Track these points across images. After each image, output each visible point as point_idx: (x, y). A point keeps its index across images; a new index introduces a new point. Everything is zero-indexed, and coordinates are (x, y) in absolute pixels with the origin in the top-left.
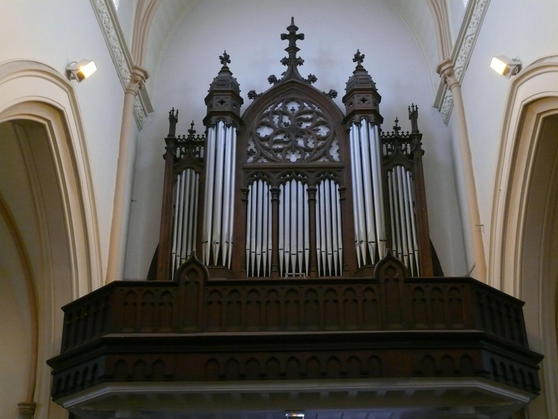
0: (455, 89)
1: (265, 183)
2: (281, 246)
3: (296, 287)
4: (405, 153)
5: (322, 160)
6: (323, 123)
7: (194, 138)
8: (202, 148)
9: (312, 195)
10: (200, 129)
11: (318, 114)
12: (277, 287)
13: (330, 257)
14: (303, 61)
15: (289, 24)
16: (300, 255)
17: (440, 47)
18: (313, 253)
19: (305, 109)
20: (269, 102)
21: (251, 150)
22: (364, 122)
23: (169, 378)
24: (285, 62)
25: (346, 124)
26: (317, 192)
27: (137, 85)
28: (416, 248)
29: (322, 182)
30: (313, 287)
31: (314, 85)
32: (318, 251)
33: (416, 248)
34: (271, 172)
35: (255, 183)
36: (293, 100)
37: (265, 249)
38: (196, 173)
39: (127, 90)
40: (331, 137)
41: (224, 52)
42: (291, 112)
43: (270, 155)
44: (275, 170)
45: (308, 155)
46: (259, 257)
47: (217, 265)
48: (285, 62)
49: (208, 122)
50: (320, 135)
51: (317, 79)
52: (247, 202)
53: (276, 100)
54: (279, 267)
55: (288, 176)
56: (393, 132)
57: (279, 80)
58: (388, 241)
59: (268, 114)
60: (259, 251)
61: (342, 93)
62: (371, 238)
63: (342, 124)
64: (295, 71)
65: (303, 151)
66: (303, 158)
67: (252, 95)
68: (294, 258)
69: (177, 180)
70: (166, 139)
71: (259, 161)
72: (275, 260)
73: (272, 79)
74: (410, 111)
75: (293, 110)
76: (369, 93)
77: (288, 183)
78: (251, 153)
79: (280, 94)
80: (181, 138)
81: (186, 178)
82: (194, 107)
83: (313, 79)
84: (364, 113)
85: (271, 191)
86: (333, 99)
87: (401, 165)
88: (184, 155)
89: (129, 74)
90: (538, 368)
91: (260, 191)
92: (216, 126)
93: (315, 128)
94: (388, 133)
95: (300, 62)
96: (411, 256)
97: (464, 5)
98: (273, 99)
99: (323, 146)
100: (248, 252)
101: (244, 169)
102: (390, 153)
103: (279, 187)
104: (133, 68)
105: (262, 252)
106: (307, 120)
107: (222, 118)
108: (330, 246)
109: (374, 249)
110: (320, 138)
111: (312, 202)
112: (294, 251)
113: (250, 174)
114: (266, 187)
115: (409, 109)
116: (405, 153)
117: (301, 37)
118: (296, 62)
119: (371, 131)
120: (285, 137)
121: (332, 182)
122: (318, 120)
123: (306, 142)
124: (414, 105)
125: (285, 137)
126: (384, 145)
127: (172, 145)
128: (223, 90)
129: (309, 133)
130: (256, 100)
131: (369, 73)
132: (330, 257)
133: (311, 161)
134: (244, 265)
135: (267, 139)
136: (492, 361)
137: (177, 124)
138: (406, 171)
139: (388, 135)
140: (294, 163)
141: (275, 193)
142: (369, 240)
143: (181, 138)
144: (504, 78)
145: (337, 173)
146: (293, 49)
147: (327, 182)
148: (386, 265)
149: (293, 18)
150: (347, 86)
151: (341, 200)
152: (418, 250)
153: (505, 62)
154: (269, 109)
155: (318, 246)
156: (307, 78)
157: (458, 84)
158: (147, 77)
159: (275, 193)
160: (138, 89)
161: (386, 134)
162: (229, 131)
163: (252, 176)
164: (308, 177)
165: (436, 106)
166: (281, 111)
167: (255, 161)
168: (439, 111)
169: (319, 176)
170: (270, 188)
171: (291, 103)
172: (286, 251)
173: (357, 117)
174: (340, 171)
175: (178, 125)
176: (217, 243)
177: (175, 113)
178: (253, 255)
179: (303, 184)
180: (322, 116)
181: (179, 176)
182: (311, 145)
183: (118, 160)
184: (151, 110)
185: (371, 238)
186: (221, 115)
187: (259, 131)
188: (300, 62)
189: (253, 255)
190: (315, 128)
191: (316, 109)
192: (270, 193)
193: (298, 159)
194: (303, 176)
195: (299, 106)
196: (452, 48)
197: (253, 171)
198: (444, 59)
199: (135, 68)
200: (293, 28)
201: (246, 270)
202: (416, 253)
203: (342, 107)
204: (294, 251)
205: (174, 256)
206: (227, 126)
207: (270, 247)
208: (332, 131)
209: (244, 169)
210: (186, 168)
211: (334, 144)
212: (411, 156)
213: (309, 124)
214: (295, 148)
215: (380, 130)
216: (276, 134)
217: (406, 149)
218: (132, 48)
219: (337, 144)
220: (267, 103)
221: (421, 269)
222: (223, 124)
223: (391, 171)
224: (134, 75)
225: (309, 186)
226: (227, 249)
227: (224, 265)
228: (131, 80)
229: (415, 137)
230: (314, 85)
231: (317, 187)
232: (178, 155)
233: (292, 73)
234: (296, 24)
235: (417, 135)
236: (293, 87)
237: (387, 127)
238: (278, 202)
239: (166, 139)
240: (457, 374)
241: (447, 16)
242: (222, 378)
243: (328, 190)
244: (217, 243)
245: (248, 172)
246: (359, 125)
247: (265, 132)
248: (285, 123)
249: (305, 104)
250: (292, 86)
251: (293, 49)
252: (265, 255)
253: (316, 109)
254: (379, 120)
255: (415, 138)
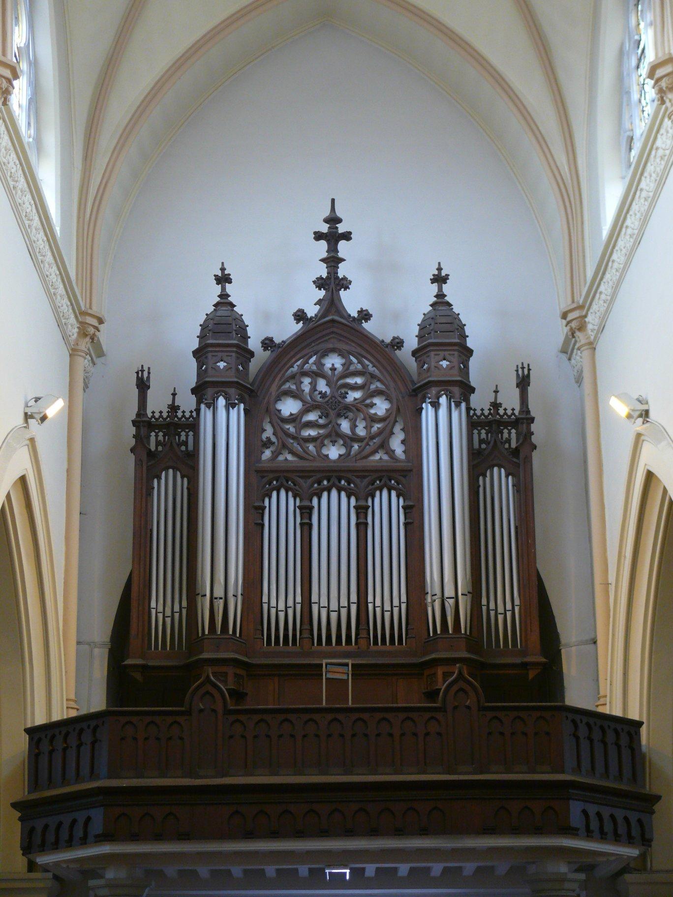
0: (586, 353)
1: (290, 494)
2: (314, 598)
3: (340, 716)
4: (507, 446)
5: (377, 457)
6: (378, 393)
7: (176, 416)
8: (191, 433)
9: (362, 515)
10: (187, 403)
11: (373, 376)
12: (316, 717)
13: (387, 615)
14: (350, 282)
15: (327, 213)
16: (344, 612)
17: (569, 275)
18: (363, 608)
19: (352, 368)
20: (297, 353)
21: (268, 439)
22: (443, 400)
23: (184, 836)
24: (320, 283)
25: (416, 395)
26: (370, 510)
27: (88, 339)
28: (517, 602)
29: (378, 493)
30: (362, 716)
31: (366, 326)
32: (370, 606)
33: (517, 602)
34: (299, 477)
35: (274, 494)
36: (333, 350)
37: (290, 603)
38: (182, 477)
39: (72, 349)
40: (392, 418)
41: (220, 266)
42: (330, 372)
43: (297, 448)
44: (305, 473)
45: (356, 446)
46: (282, 615)
47: (220, 630)
48: (320, 283)
49: (198, 391)
50: (376, 414)
51: (371, 316)
52: (262, 526)
53: (307, 351)
54: (312, 630)
55: (325, 482)
56: (490, 410)
57: (311, 318)
58: (475, 592)
59: (293, 377)
60: (281, 606)
61: (412, 342)
62: (449, 591)
63: (410, 396)
64: (336, 301)
65: (348, 441)
66: (348, 454)
67: (268, 343)
68: (334, 616)
69: (153, 488)
70: (133, 421)
71: (281, 458)
72: (306, 620)
73: (300, 316)
74: (518, 375)
75: (333, 369)
76: (454, 350)
77: (325, 494)
78: (268, 443)
79: (314, 341)
80: (157, 415)
81: (167, 487)
82: (176, 375)
83: (365, 315)
84: (445, 385)
85: (300, 508)
86: (397, 352)
87: (500, 466)
88: (162, 445)
89: (77, 325)
90: (652, 812)
91: (282, 506)
92: (212, 405)
93: (368, 401)
94: (482, 410)
95: (344, 284)
96: (509, 614)
97: (601, 232)
98: (303, 349)
99: (380, 432)
100: (265, 606)
101: (257, 471)
102: (484, 446)
103: (311, 501)
104: (80, 313)
105: (286, 607)
106: (355, 388)
107: (223, 391)
108: (388, 598)
109: (453, 610)
110: (374, 419)
111: (362, 527)
112: (334, 606)
113: (265, 480)
114: (291, 500)
115: (517, 371)
116: (507, 446)
117: (347, 236)
118: (338, 285)
119: (455, 414)
120: (320, 417)
121: (394, 493)
122: (373, 387)
123: (354, 427)
124: (526, 366)
125: (320, 417)
126: (475, 432)
127: (143, 431)
128: (223, 331)
129: (358, 410)
130: (275, 354)
131: (456, 310)
132: (387, 615)
133: (361, 459)
134: (260, 628)
135: (293, 419)
136: (585, 812)
137: (149, 391)
138: (507, 477)
139: (483, 414)
140: (334, 461)
141: (306, 511)
142: (446, 595)
143: (157, 415)
144: (628, 421)
145: (401, 478)
146: (333, 261)
147: (385, 493)
148: (455, 688)
149: (333, 201)
150: (420, 330)
151: (406, 524)
152: (520, 606)
153: (628, 406)
154: (295, 368)
155: (370, 599)
156: (356, 315)
157: (592, 346)
158: (101, 321)
159: (306, 511)
160: (89, 345)
161: (479, 413)
162: (233, 413)
163: (270, 483)
164: (355, 485)
165: (564, 351)
166: (313, 372)
167: (275, 455)
168: (569, 359)
169: (373, 484)
170: (298, 504)
171: (331, 355)
172: (322, 605)
173: (434, 391)
174: (405, 477)
175: (150, 392)
176: (221, 598)
177: (145, 374)
178: (273, 611)
179: (349, 498)
180: (379, 380)
181: (156, 481)
182: (361, 431)
183: (68, 471)
184: (101, 353)
185: (449, 591)
186: (221, 387)
187: (280, 406)
188: (344, 284)
189: (273, 611)
190: (368, 401)
191: (371, 368)
192: (298, 511)
193: (340, 456)
194: (349, 484)
195: (343, 361)
196: (585, 284)
197: (271, 476)
198: (573, 302)
199: (84, 313)
200: (333, 220)
201: (263, 635)
202: (517, 609)
203: (411, 364)
204: (334, 606)
205: (153, 611)
206: (230, 405)
207: (299, 599)
208: (395, 407)
209: (257, 471)
210: (166, 469)
211: (397, 429)
212: (516, 452)
213: (358, 395)
214: (335, 435)
215: (468, 409)
216: (306, 410)
217: (509, 441)
218: (77, 274)
219: (403, 430)
220: (292, 358)
221: (523, 636)
222: (224, 401)
223: (485, 476)
224: (83, 326)
225: (357, 500)
226: (235, 607)
227: (231, 632)
228: (79, 333)
229: (523, 421)
230: (366, 326)
231: (370, 503)
232: (153, 447)
233: (331, 304)
234: (339, 213)
235: (527, 419)
236: (335, 330)
237: (480, 401)
238: (310, 526)
239: (133, 421)
240: (539, 831)
241: (582, 223)
242: (249, 835)
243: (386, 506)
244: (221, 598)
245: (263, 477)
246: (436, 405)
247: (289, 407)
248: (320, 393)
249: (352, 358)
250: (332, 326)
251: (333, 261)
252: (290, 612)
253: (371, 368)
254: (467, 390)
255: (522, 423)
